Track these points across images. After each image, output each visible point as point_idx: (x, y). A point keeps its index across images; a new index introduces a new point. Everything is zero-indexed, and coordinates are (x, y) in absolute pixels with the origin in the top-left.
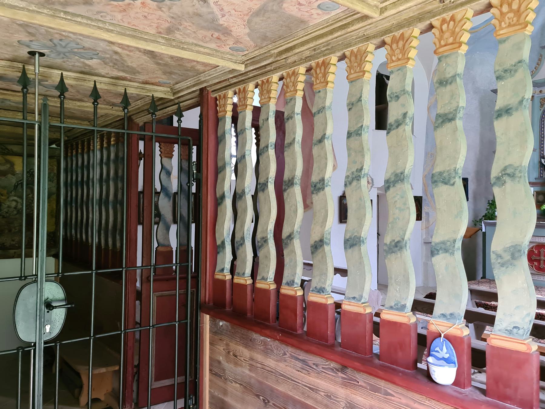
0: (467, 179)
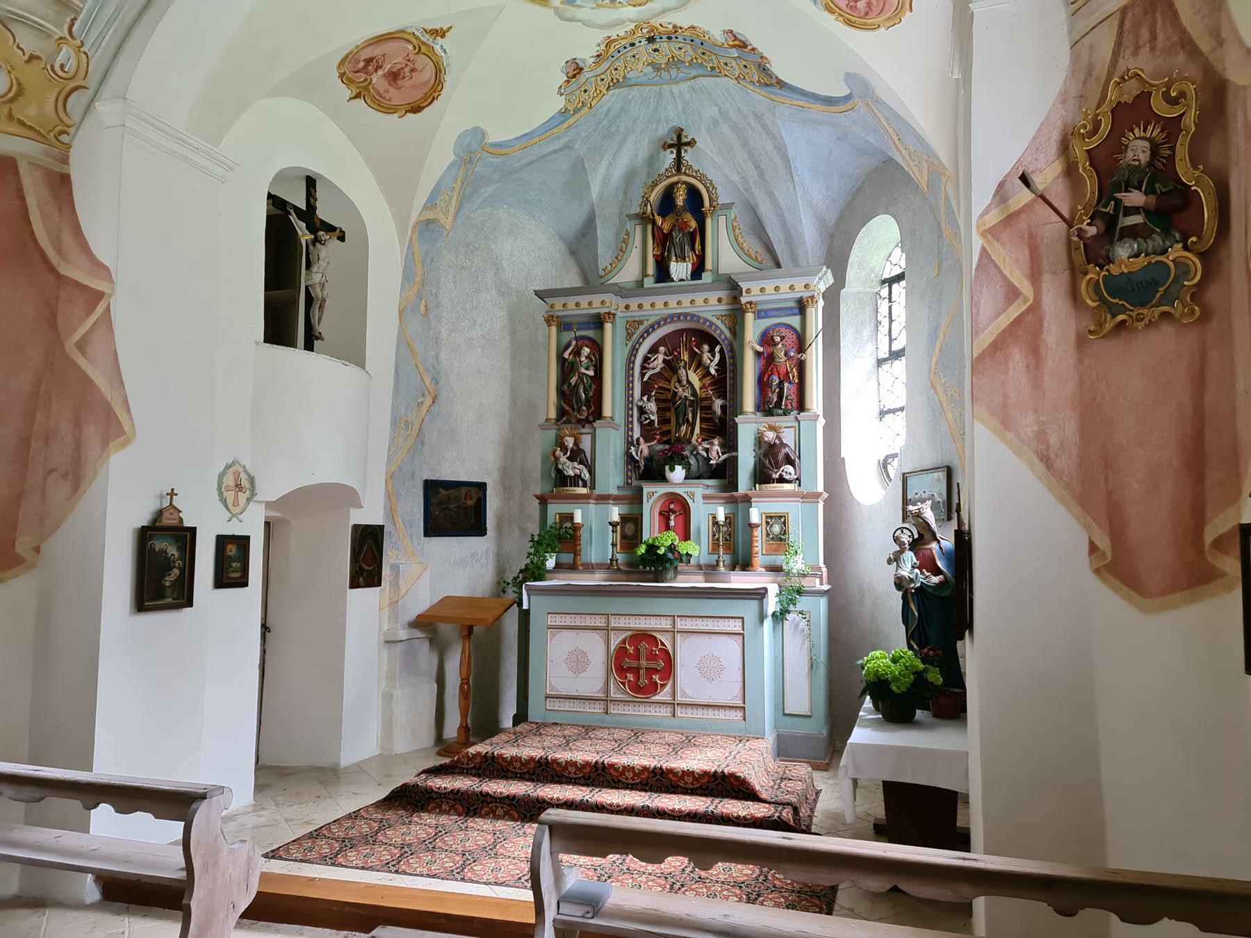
0: (485, 484)
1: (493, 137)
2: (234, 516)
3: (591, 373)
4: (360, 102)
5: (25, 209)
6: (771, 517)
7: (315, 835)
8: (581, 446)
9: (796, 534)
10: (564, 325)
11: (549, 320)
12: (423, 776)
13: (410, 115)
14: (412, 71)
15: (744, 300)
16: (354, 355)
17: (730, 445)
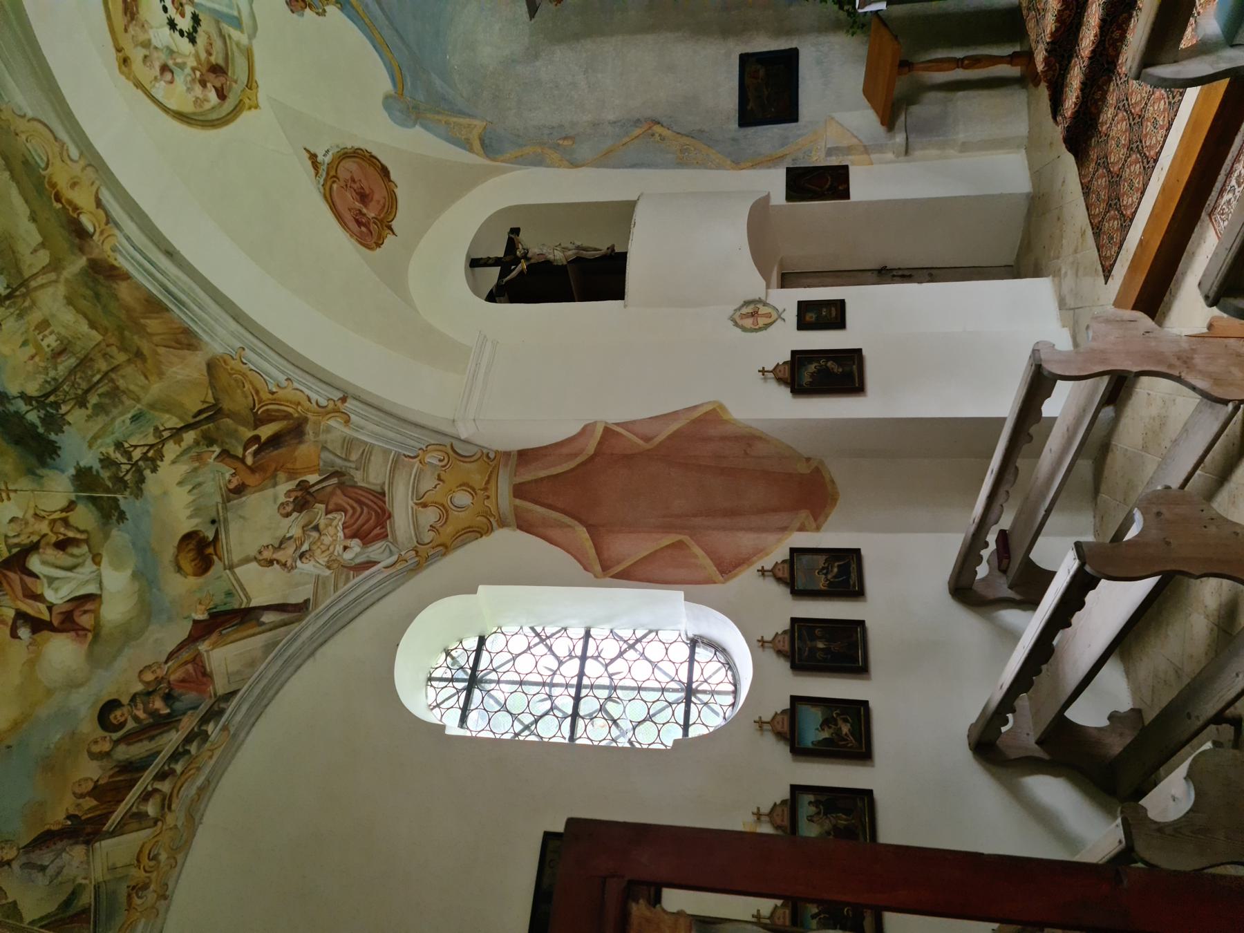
1: (387, 86)
2: (779, 316)
4: (394, 224)
5: (548, 477)
7: (1097, 231)
12: (1059, 119)
13: (393, 177)
14: (353, 181)
16: (624, 212)
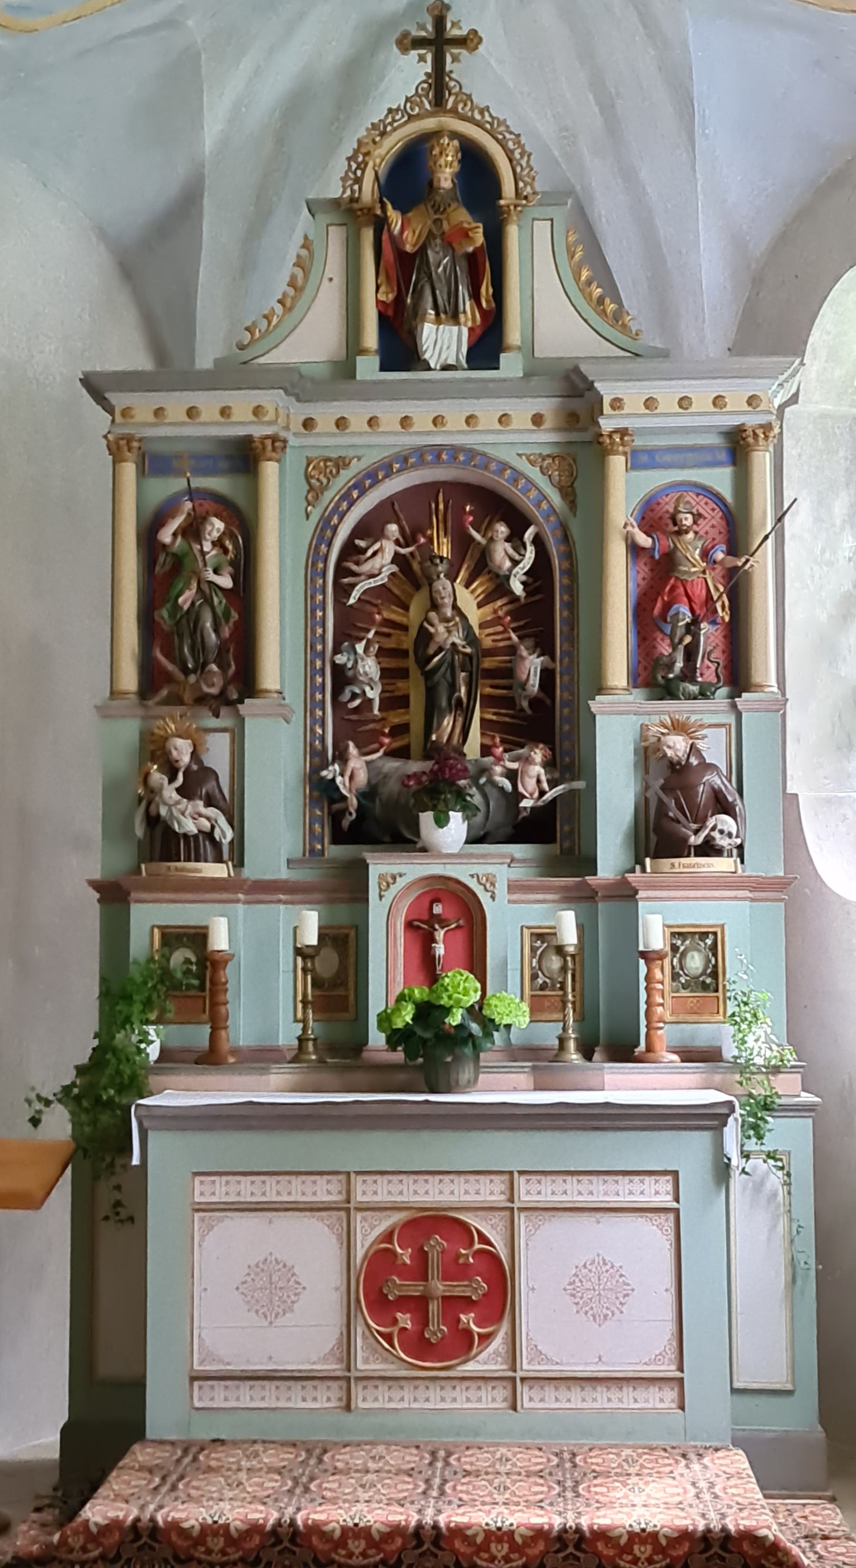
3: (226, 582)
6: (682, 935)
8: (208, 762)
9: (737, 972)
10: (153, 463)
11: (117, 449)
15: (606, 424)
17: (572, 761)
